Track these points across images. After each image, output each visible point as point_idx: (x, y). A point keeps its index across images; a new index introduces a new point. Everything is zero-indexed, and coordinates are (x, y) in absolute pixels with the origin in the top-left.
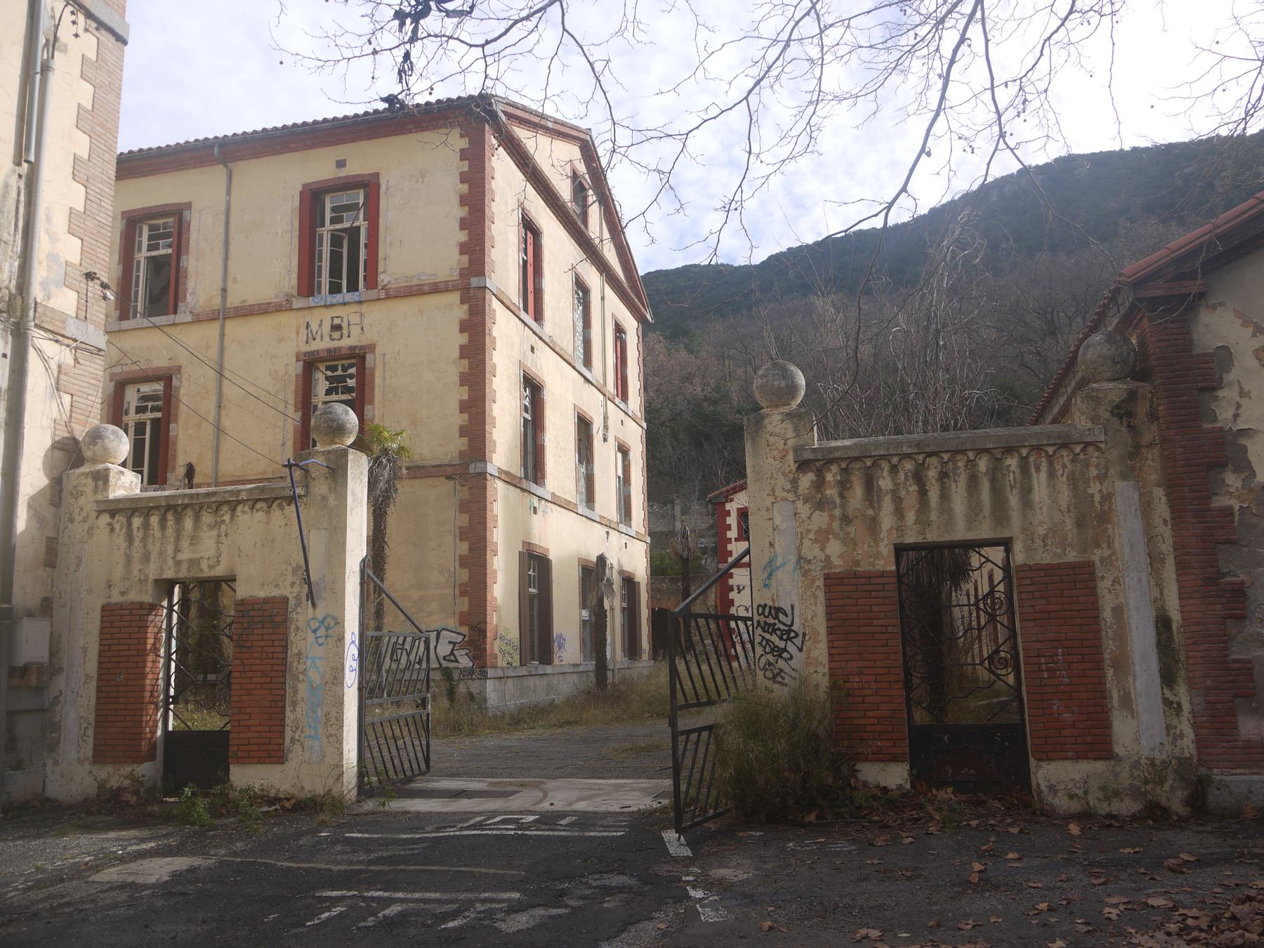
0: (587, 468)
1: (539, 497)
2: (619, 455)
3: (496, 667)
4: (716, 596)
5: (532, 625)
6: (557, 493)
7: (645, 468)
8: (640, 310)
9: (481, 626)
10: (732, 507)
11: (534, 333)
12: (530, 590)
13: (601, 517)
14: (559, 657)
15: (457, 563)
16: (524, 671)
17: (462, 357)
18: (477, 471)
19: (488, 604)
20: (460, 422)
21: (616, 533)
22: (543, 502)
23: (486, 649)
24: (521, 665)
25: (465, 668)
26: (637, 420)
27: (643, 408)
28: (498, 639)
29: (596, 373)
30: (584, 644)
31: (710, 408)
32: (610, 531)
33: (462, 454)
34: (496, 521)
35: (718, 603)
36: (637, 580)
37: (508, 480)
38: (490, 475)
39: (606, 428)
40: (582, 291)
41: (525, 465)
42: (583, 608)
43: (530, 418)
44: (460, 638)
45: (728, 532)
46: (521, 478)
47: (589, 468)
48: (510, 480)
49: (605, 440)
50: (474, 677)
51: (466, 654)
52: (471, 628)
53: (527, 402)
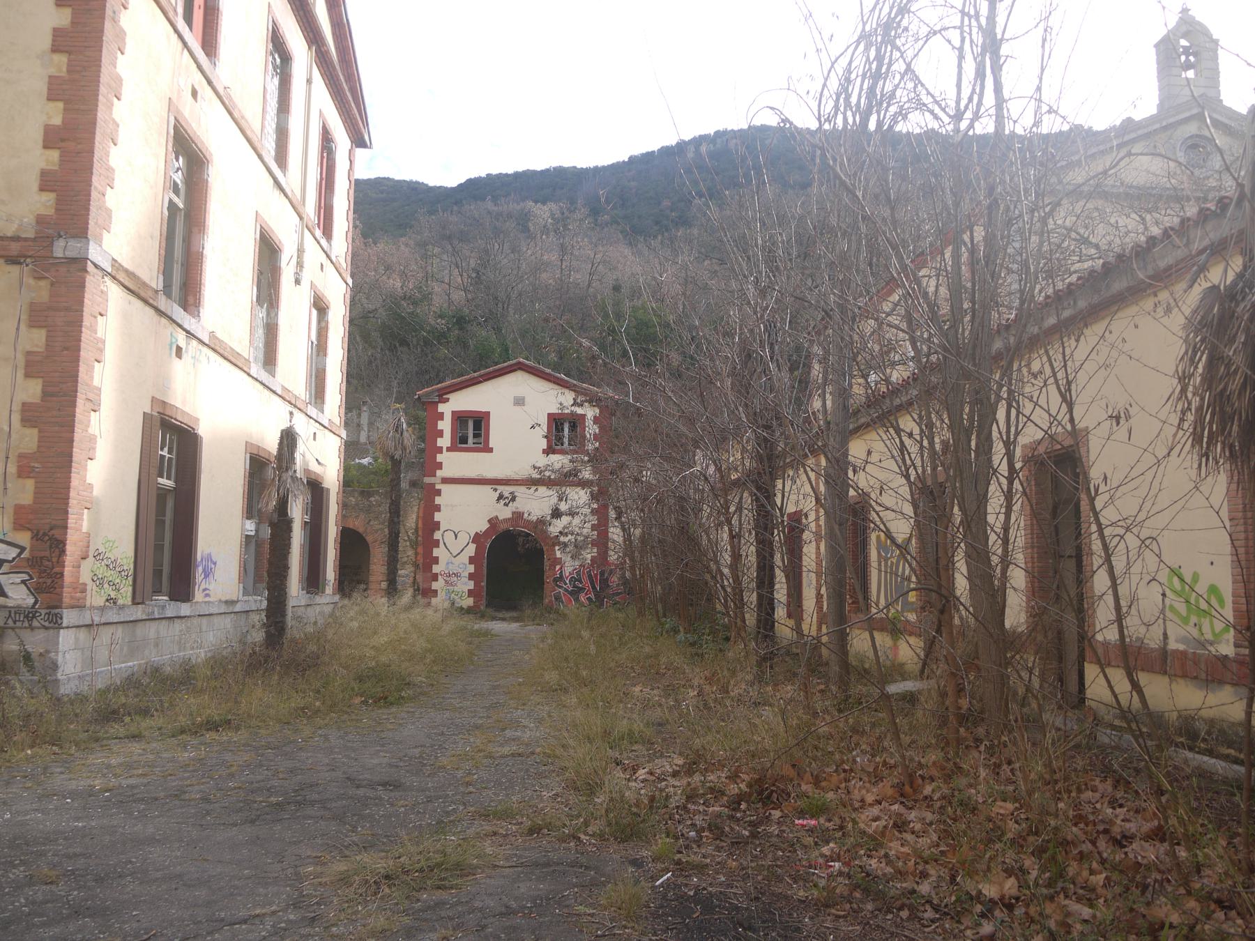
0: (268, 314)
1: (188, 332)
2: (315, 312)
3: (81, 607)
4: (418, 517)
5: (159, 536)
6: (219, 335)
7: (346, 339)
8: (357, 124)
9: (56, 533)
10: (446, 409)
11: (199, 67)
12: (160, 480)
13: (284, 388)
14: (205, 590)
15: (16, 418)
16: (138, 613)
17: (55, 49)
18: (69, 254)
19: (72, 494)
20: (43, 165)
21: (303, 416)
22: (194, 343)
23: (62, 575)
24: (135, 602)
25: (19, 607)
26: (342, 271)
27: (349, 259)
28: (91, 559)
29: (292, 180)
30: (245, 570)
31: (407, 308)
32: (295, 411)
33: (40, 220)
34: (101, 350)
35: (420, 525)
36: (325, 485)
37: (131, 287)
38: (96, 266)
39: (300, 265)
40: (280, 57)
41: (167, 272)
42: (248, 518)
43: (181, 206)
44: (13, 553)
45: (439, 439)
46: (156, 292)
47: (273, 315)
48: (135, 289)
49: (298, 282)
50: (35, 623)
51: (23, 582)
52: (36, 537)
53: (178, 178)
